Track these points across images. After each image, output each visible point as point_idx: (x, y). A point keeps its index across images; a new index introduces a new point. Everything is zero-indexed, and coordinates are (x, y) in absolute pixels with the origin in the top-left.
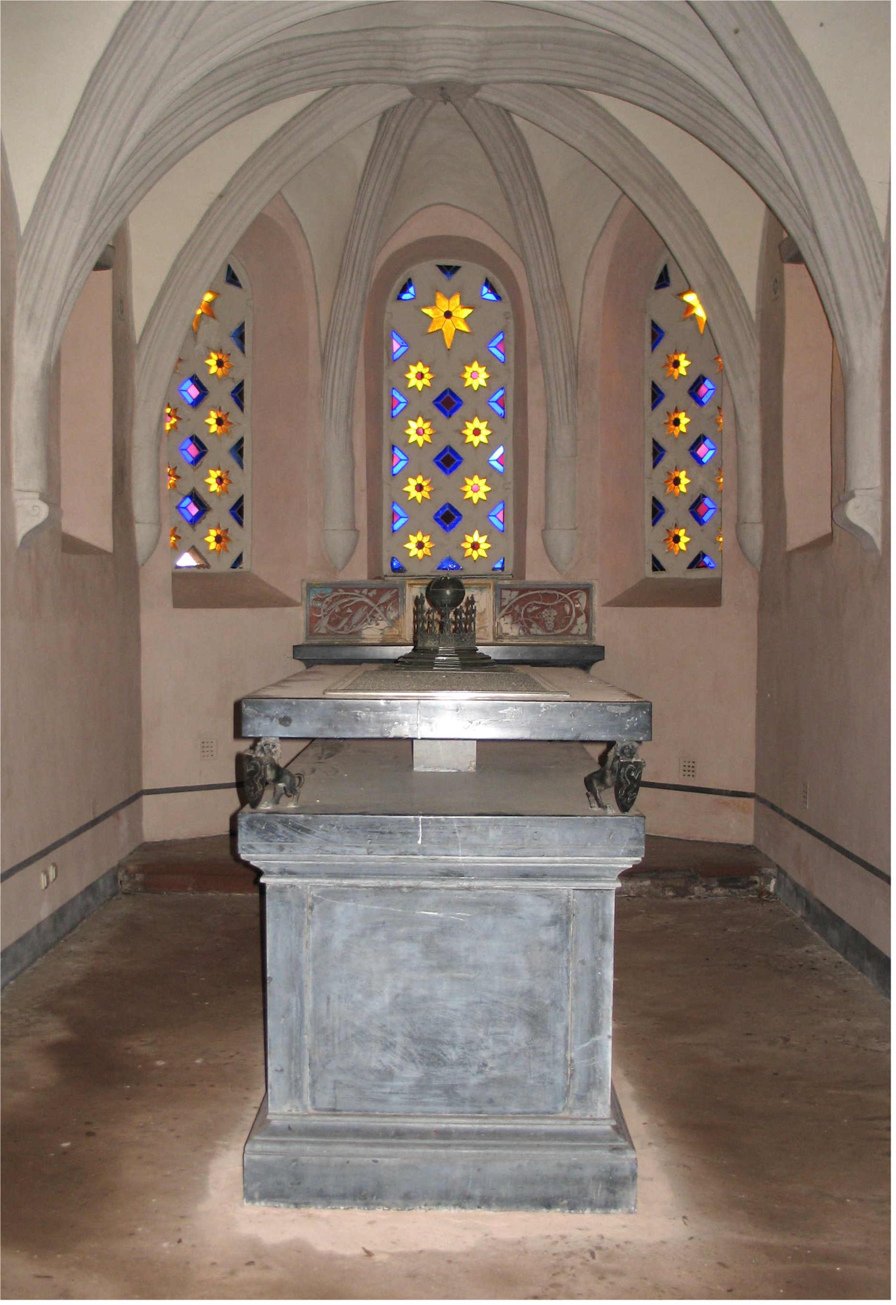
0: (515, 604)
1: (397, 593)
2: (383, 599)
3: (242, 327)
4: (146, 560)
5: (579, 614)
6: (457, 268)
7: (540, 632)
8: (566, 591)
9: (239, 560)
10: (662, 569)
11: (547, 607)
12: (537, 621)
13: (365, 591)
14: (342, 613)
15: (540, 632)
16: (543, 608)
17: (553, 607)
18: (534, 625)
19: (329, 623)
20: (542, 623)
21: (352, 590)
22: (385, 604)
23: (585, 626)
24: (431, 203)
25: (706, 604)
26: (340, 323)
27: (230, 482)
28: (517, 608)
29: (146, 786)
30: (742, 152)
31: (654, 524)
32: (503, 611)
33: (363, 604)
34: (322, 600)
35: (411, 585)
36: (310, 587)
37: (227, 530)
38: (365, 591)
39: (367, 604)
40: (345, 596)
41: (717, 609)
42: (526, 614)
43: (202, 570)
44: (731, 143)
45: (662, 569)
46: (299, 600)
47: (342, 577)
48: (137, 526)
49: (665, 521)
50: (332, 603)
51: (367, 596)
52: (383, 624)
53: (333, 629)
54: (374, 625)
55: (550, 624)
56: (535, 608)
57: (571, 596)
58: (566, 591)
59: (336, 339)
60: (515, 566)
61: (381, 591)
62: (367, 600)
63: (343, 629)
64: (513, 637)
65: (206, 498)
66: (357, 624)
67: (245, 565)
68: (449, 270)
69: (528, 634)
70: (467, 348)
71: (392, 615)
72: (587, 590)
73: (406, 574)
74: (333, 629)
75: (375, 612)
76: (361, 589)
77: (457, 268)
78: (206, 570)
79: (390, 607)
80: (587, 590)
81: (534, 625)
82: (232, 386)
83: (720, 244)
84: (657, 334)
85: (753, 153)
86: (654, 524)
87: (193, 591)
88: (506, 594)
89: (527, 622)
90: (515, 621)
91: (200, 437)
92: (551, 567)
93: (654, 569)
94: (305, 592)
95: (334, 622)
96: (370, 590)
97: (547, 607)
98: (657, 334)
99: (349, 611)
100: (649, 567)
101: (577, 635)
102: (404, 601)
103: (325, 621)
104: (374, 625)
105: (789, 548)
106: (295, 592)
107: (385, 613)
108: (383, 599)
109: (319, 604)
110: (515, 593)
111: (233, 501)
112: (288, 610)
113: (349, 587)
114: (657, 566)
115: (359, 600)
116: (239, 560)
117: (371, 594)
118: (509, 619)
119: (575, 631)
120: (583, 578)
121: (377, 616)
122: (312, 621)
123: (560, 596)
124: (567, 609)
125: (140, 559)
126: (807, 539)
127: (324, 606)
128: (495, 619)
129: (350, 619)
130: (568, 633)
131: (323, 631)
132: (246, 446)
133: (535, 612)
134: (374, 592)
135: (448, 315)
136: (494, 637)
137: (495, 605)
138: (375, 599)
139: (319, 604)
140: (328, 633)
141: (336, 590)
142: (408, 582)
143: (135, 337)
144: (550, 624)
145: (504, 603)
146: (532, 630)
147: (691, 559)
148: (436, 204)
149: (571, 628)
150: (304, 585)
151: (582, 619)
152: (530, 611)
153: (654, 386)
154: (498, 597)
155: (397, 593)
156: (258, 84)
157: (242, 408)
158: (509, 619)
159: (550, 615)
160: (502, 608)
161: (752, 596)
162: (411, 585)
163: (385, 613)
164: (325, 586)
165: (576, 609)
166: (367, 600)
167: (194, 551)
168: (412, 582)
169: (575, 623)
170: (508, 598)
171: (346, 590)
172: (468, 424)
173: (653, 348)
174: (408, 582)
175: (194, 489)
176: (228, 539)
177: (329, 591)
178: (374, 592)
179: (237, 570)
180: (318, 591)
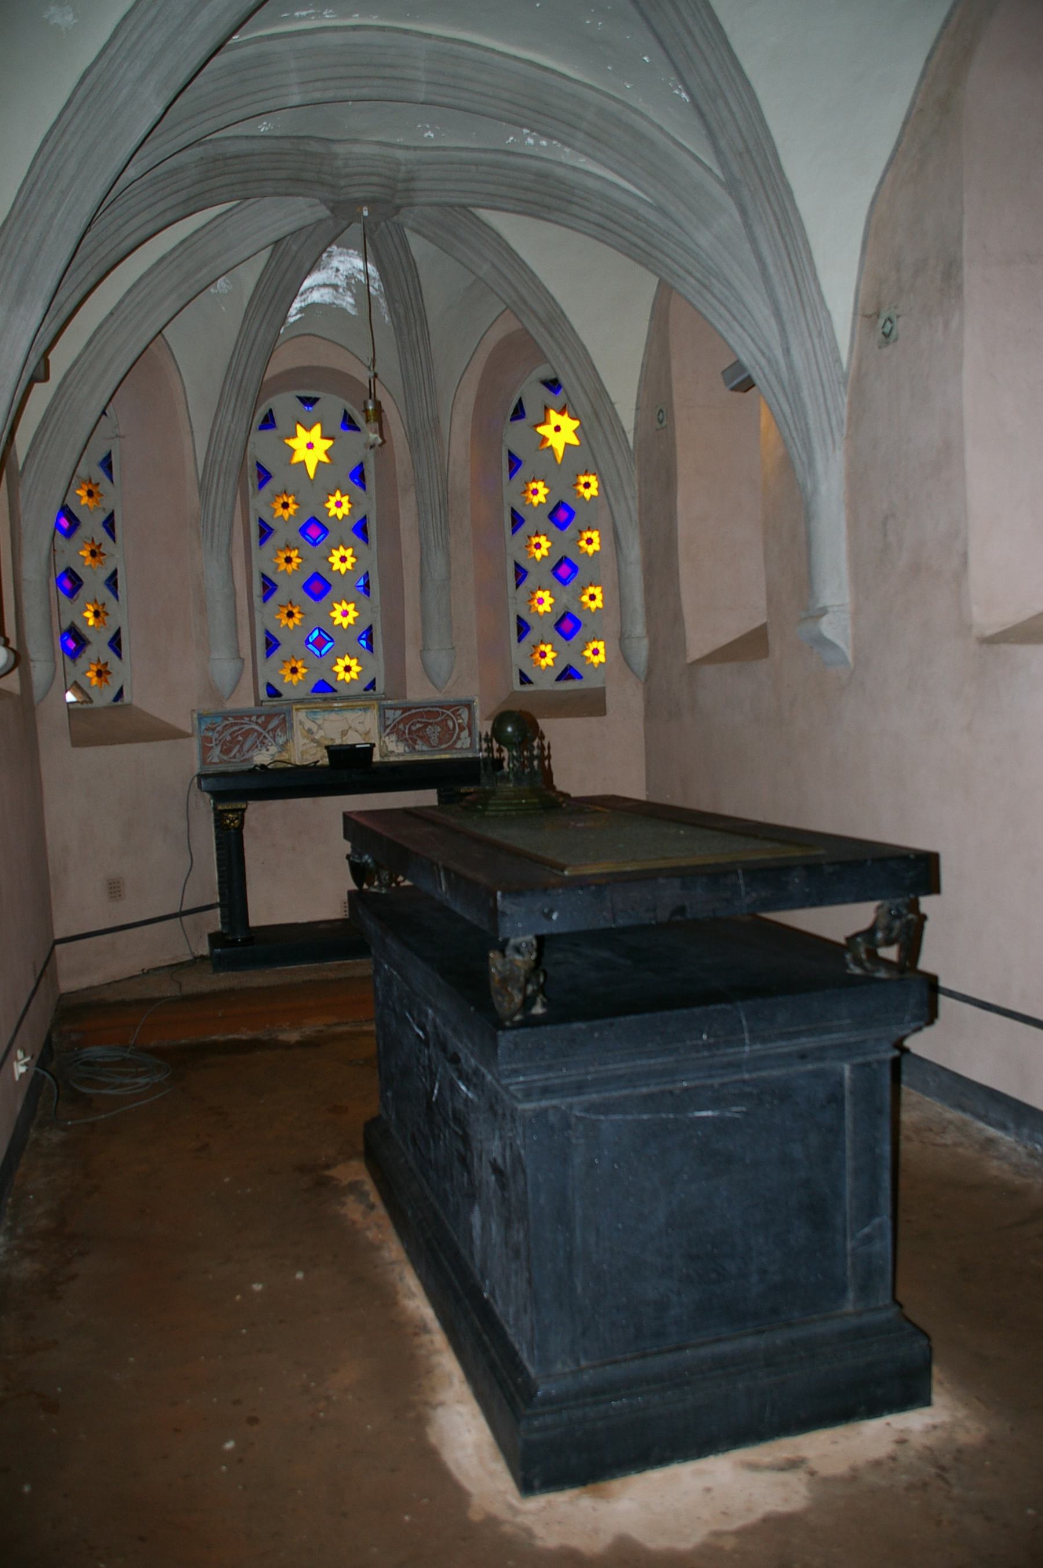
0: (399, 723)
1: (284, 718)
2: (271, 726)
3: (109, 455)
4: (41, 700)
5: (462, 729)
6: (316, 400)
7: (425, 748)
8: (449, 707)
9: (120, 694)
10: (530, 682)
11: (431, 724)
12: (421, 738)
13: (254, 718)
14: (234, 741)
15: (425, 748)
16: (426, 725)
17: (436, 723)
18: (419, 742)
19: (221, 751)
20: (426, 740)
21: (242, 718)
22: (274, 730)
23: (469, 740)
24: (303, 332)
25: (591, 714)
26: (221, 452)
27: (107, 614)
28: (401, 727)
29: (58, 935)
30: (693, 281)
31: (519, 640)
32: (388, 731)
33: (253, 730)
34: (213, 730)
35: (297, 710)
36: (201, 717)
37: (106, 664)
38: (254, 718)
39: (256, 731)
40: (235, 724)
41: (602, 718)
42: (410, 732)
43: (85, 706)
44: (681, 272)
45: (530, 682)
46: (190, 731)
47: (230, 706)
48: (32, 664)
49: (530, 637)
50: (222, 732)
51: (257, 723)
52: (273, 749)
53: (225, 758)
54: (264, 751)
55: (434, 740)
56: (419, 726)
57: (453, 713)
58: (449, 707)
59: (217, 468)
60: (385, 686)
61: (270, 717)
62: (256, 727)
63: (234, 757)
64: (399, 755)
65: (85, 632)
66: (248, 751)
67: (127, 698)
68: (309, 402)
69: (413, 750)
70: (326, 480)
71: (281, 740)
72: (469, 705)
73: (283, 698)
74: (225, 758)
75: (265, 737)
76: (250, 716)
77: (316, 400)
78: (90, 706)
79: (278, 732)
80: (469, 705)
81: (419, 742)
82: (103, 516)
83: (31, 436)
84: (515, 463)
85: (706, 282)
86: (519, 640)
87: (91, 727)
88: (389, 713)
89: (411, 739)
90: (401, 738)
91: (75, 570)
92: (431, 685)
93: (522, 683)
94: (196, 722)
95: (226, 751)
96: (258, 717)
97: (431, 724)
98: (515, 463)
99: (240, 738)
100: (516, 678)
101: (461, 748)
102: (292, 726)
103: (217, 751)
104: (264, 751)
105: (689, 660)
106: (185, 724)
107: (274, 738)
108: (271, 726)
109: (210, 734)
110: (399, 712)
111: (110, 634)
112: (180, 741)
113: (239, 716)
114: (524, 679)
115: (247, 727)
116: (120, 694)
117: (260, 721)
118: (394, 738)
119: (458, 745)
120: (463, 695)
121: (266, 741)
122: (205, 750)
123: (443, 713)
124: (450, 724)
125: (36, 700)
126: (706, 651)
127: (216, 735)
128: (380, 738)
129: (242, 746)
130: (452, 747)
131: (216, 760)
132: (120, 577)
133: (419, 730)
134: (263, 718)
135: (310, 446)
136: (381, 756)
137: (379, 727)
138: (264, 726)
139: (210, 734)
140: (222, 762)
141: (226, 718)
142: (294, 707)
143: (17, 462)
144: (434, 740)
145: (388, 723)
146: (417, 747)
147: (559, 672)
148: (305, 335)
149: (455, 742)
150: (195, 716)
151: (465, 733)
152: (414, 728)
153: (513, 511)
154: (382, 717)
155: (284, 718)
156: (194, 184)
157: (114, 538)
158: (394, 738)
159: (434, 732)
160: (386, 727)
161: (637, 703)
162: (297, 710)
163: (274, 738)
164: (216, 715)
165: (459, 724)
166: (256, 727)
167: (77, 687)
168: (299, 706)
169: (458, 738)
170: (392, 717)
171: (235, 718)
172: (341, 548)
173: (511, 476)
174: (294, 707)
175: (73, 623)
176: (109, 673)
177: (219, 720)
178: (263, 718)
179: (119, 703)
180: (209, 720)
